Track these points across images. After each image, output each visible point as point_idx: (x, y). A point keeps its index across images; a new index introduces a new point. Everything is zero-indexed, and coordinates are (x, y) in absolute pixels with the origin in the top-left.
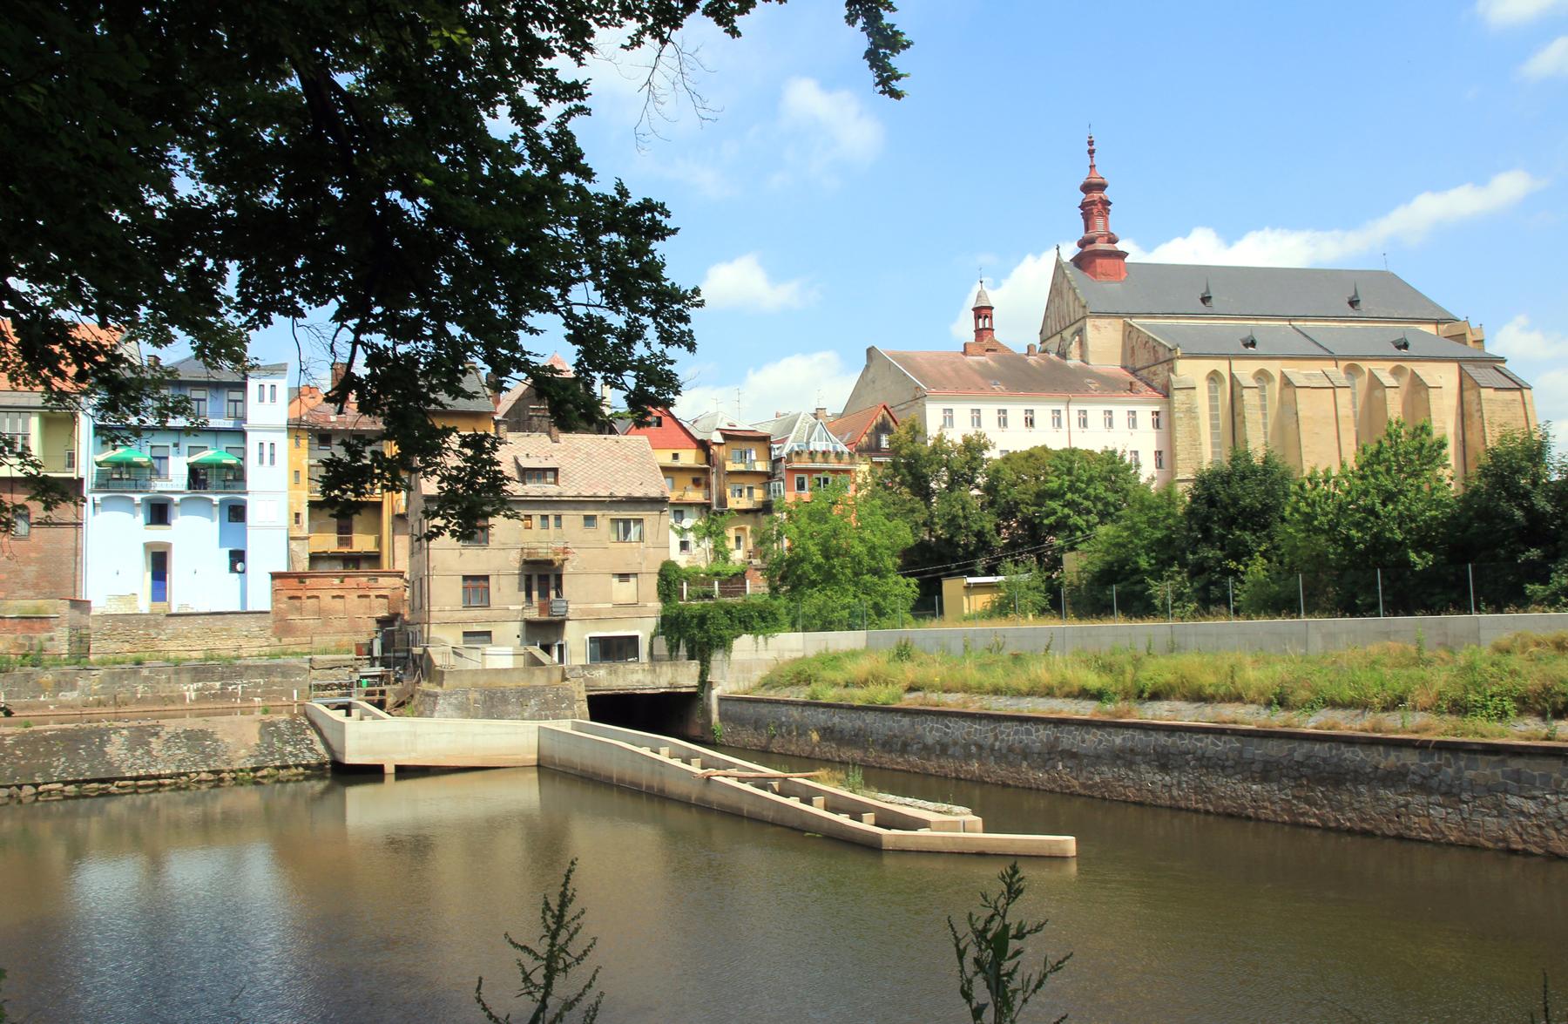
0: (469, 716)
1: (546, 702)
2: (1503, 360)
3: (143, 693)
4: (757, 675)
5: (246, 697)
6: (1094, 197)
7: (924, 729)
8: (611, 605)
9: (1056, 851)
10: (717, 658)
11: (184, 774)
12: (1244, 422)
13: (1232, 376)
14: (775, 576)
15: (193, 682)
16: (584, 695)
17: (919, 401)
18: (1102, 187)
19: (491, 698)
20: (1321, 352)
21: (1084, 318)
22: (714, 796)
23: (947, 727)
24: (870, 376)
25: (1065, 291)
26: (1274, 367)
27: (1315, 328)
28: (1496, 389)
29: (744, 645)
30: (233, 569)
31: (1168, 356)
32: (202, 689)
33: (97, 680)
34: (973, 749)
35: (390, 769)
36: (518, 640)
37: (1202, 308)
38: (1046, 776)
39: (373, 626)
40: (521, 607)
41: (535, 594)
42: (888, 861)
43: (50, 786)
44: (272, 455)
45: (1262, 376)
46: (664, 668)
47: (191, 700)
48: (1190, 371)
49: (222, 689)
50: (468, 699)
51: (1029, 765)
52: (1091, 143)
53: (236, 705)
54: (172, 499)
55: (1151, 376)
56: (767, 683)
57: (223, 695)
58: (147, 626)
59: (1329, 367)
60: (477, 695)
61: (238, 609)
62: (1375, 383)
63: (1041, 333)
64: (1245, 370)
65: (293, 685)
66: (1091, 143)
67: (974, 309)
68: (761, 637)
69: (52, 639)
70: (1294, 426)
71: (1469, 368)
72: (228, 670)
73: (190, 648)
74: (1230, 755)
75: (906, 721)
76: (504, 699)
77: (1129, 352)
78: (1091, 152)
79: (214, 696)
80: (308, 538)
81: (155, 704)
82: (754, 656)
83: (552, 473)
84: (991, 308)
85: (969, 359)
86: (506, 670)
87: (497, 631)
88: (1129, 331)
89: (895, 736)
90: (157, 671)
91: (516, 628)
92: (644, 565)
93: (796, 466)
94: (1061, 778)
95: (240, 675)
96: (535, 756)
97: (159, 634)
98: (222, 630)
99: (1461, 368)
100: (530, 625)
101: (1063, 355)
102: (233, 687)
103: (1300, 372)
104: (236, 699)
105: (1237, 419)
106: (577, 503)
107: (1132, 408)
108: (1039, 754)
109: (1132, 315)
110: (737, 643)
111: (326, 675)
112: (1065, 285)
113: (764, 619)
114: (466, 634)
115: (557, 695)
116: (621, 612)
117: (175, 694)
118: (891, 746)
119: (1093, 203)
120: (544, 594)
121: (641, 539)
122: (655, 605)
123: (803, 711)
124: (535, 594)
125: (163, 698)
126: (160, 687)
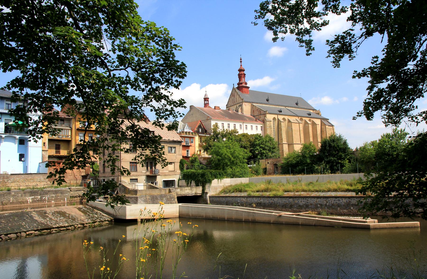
0: (147, 204)
1: (168, 199)
3: (13, 200)
4: (220, 190)
5: (49, 201)
6: (241, 74)
7: (298, 201)
9: (416, 225)
10: (207, 186)
11: (72, 225)
12: (281, 130)
13: (278, 119)
14: (349, 156)
15: (30, 196)
16: (176, 197)
17: (209, 120)
18: (244, 70)
19: (153, 198)
21: (242, 102)
22: (281, 220)
23: (307, 200)
24: (191, 113)
25: (235, 95)
26: (286, 117)
27: (291, 109)
28: (329, 126)
29: (215, 182)
30: (20, 160)
31: (264, 113)
32: (34, 198)
34: (319, 205)
35: (139, 220)
36: (145, 181)
37: (266, 102)
38: (347, 211)
39: (81, 178)
40: (145, 172)
41: (149, 168)
42: (372, 232)
43: (30, 232)
45: (284, 119)
46: (194, 188)
47: (30, 202)
48: (269, 117)
49: (41, 198)
50: (147, 198)
51: (340, 208)
52: (241, 59)
53: (46, 203)
56: (221, 192)
57: (41, 200)
58: (4, 178)
59: (297, 118)
60: (149, 197)
61: (22, 172)
62: (306, 123)
63: (227, 105)
64: (281, 117)
65: (65, 196)
66: (241, 59)
68: (219, 180)
69: (64, 177)
70: (291, 132)
71: (323, 121)
72: (43, 192)
74: (411, 202)
75: (291, 200)
76: (157, 198)
77: (252, 112)
78: (241, 62)
79: (38, 201)
80: (47, 151)
81: (17, 204)
82: (218, 185)
83: (152, 133)
84: (208, 98)
85: (216, 110)
86: (142, 190)
87: (139, 178)
88: (253, 106)
89: (287, 204)
90: (18, 193)
91: (144, 178)
92: (176, 160)
93: (182, 135)
94: (353, 211)
95: (47, 194)
96: (178, 214)
97: (8, 181)
99: (321, 121)
100: (148, 177)
101: (237, 111)
103: (292, 119)
104: (46, 201)
105: (279, 129)
107: (257, 125)
108: (344, 205)
109: (253, 103)
110: (213, 181)
111: (75, 193)
112: (236, 94)
113: (220, 175)
114: (131, 179)
115: (170, 197)
116: (171, 173)
117: (24, 200)
118: (286, 206)
119: (242, 74)
120: (151, 168)
121: (175, 152)
122: (179, 171)
123: (247, 199)
124: (149, 168)
126: (19, 198)
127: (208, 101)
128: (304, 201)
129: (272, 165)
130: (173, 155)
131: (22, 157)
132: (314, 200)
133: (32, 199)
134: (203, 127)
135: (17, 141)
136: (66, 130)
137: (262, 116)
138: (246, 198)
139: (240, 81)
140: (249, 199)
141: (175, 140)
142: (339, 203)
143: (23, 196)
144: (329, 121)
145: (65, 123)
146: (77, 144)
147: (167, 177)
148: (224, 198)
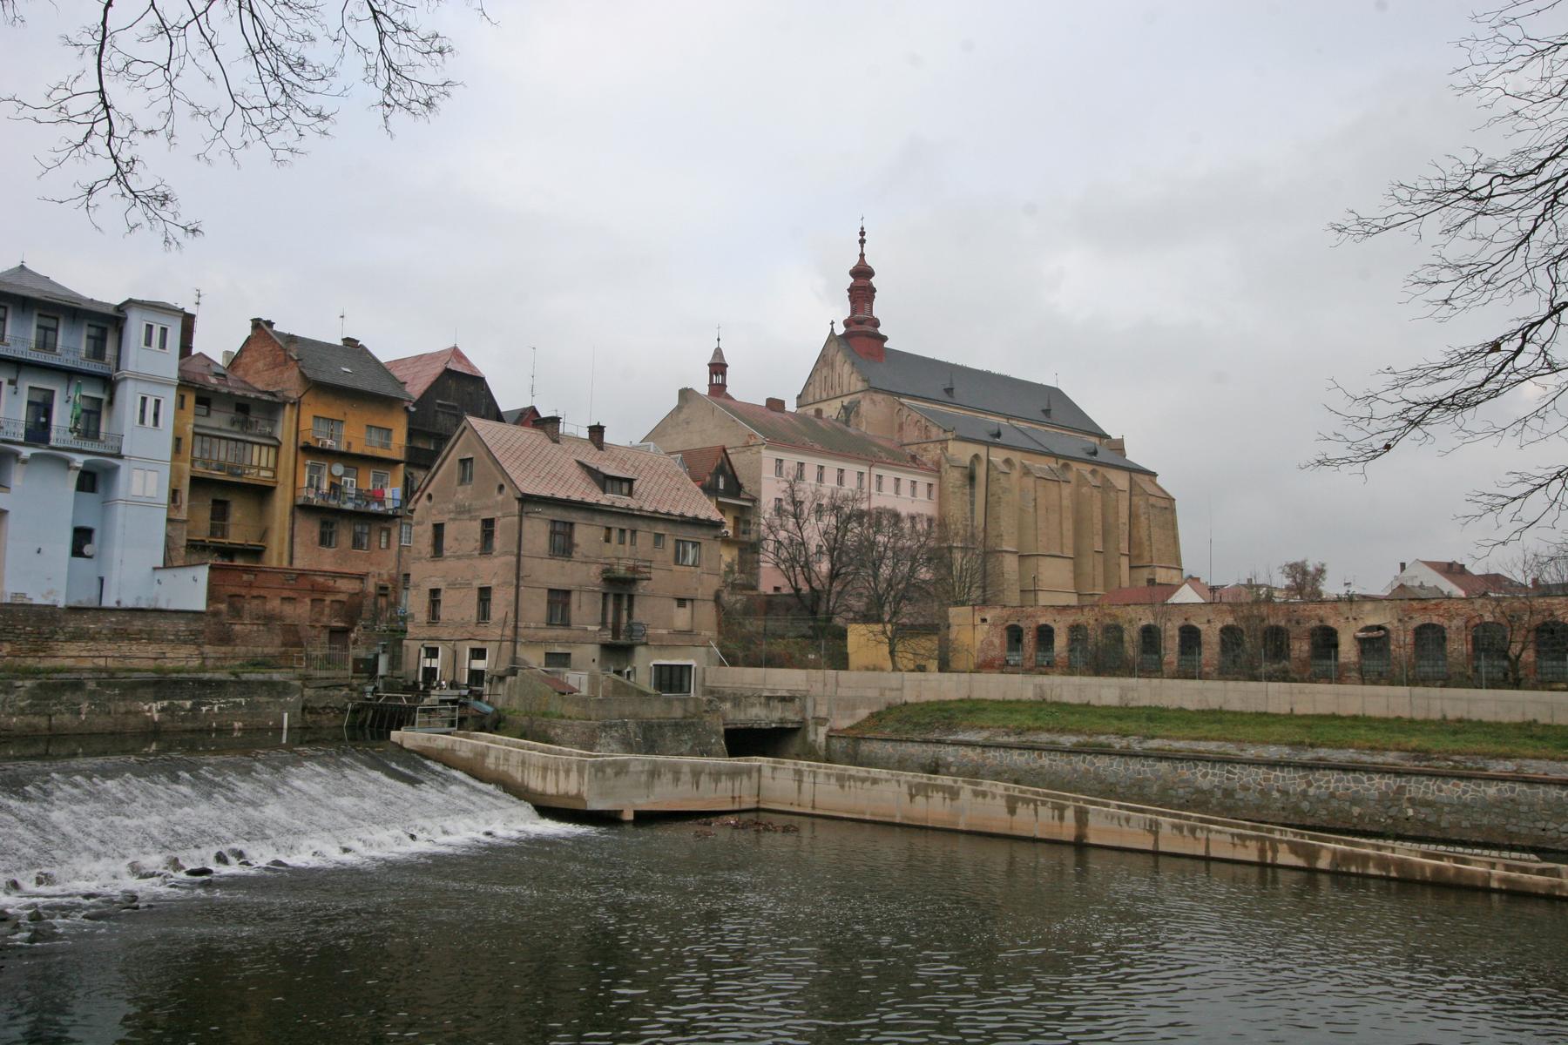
2: (1154, 475)
6: (862, 285)
7: (1194, 774)
13: (988, 460)
16: (722, 729)
20: (1033, 446)
24: (682, 416)
26: (1017, 457)
35: (629, 816)
40: (597, 628)
44: (156, 415)
52: (862, 233)
54: (21, 453)
55: (921, 452)
63: (799, 397)
66: (862, 233)
73: (97, 654)
78: (862, 242)
89: (1148, 779)
91: (593, 651)
98: (141, 631)
99: (1131, 478)
100: (607, 649)
106: (653, 518)
109: (900, 395)
123: (984, 752)
127: (724, 374)
128: (1214, 775)
129: (999, 629)
131: (82, 537)
132: (1257, 774)
133: (163, 710)
134: (730, 473)
135: (73, 478)
136: (200, 438)
138: (979, 750)
139: (853, 311)
140: (991, 753)
141: (701, 517)
142: (1357, 792)
144: (236, 350)
145: (212, 413)
146: (300, 501)
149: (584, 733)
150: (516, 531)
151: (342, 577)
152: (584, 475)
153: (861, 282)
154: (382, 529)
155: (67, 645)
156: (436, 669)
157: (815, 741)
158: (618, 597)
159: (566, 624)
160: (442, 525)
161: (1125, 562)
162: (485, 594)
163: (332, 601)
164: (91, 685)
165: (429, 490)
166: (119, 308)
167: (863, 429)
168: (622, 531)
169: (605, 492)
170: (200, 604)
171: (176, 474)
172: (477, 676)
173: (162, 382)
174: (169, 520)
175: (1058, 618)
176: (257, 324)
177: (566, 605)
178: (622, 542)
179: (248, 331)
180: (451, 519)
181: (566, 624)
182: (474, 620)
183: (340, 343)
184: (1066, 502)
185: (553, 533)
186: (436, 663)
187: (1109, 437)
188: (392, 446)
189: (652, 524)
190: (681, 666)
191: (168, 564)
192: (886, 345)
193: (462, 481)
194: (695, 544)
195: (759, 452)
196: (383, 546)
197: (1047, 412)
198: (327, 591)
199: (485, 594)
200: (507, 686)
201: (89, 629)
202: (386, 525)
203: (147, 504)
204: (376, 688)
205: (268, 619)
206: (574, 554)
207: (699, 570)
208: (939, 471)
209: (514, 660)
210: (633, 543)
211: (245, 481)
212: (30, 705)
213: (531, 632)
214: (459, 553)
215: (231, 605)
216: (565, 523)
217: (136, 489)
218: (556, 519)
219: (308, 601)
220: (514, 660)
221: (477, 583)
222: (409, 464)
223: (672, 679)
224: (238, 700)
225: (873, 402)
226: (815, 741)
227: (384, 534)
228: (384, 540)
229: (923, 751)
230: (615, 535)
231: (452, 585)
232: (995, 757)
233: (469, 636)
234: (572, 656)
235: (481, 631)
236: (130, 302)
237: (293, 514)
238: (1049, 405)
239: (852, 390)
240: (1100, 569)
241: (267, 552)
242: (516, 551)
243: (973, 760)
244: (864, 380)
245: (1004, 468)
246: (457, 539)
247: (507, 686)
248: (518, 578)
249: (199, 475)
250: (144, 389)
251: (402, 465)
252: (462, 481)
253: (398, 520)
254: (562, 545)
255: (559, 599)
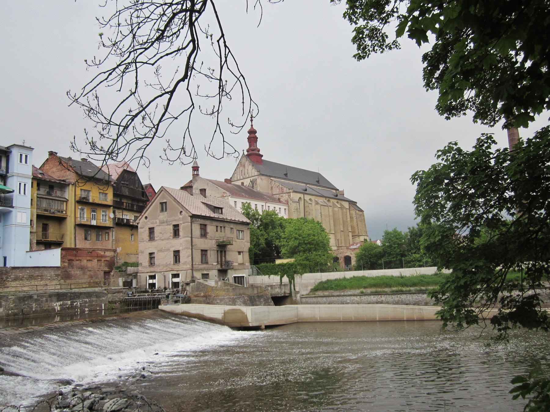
2: (356, 203)
8: (237, 264)
15: (58, 301)
17: (226, 198)
25: (246, 165)
26: (313, 198)
33: (12, 302)
35: (263, 327)
40: (216, 264)
49: (71, 304)
67: (193, 167)
79: (68, 308)
98: (38, 276)
102: (76, 303)
109: (270, 176)
114: (202, 274)
117: (50, 308)
125: (45, 310)
127: (198, 170)
130: (242, 242)
133: (60, 305)
137: (284, 195)
138: (358, 297)
139: (250, 146)
143: (48, 301)
147: (237, 272)
148: (325, 298)
149: (230, 301)
150: (190, 228)
151: (107, 251)
152: (205, 207)
153: (252, 135)
154: (106, 233)
155: (12, 283)
156: (155, 283)
157: (296, 300)
158: (221, 252)
159: (207, 263)
160: (153, 228)
161: (350, 234)
162: (177, 253)
163: (104, 261)
164: (35, 297)
165: (146, 215)
166: (8, 148)
167: (258, 189)
168: (221, 227)
169: (215, 213)
170: (58, 264)
171: (32, 215)
172: (176, 285)
173: (26, 177)
174: (31, 232)
175: (352, 253)
176: (51, 154)
177: (206, 255)
178: (221, 231)
179: (47, 156)
180: (157, 226)
181: (207, 263)
182: (172, 263)
183: (80, 160)
184: (331, 214)
185: (201, 228)
186: (154, 281)
187: (338, 190)
188: (108, 200)
189: (229, 224)
190: (241, 277)
191: (31, 250)
192: (263, 158)
193: (162, 210)
194: (242, 231)
195: (228, 199)
196: (107, 239)
197: (318, 182)
198: (102, 256)
199: (177, 253)
200: (191, 287)
201: (20, 276)
202: (108, 231)
203: (23, 226)
204: (133, 292)
205: (82, 268)
206: (207, 236)
207: (244, 241)
208: (288, 204)
209: (193, 277)
210: (225, 232)
211: (56, 215)
212: (15, 306)
213: (197, 266)
214: (163, 238)
215: (69, 264)
216: (204, 225)
217: (19, 221)
218: (202, 223)
219: (96, 260)
220: (193, 277)
221: (173, 249)
222: (115, 207)
223: (239, 280)
224: (86, 300)
225: (262, 179)
226: (296, 300)
227: (107, 235)
228: (107, 237)
229: (338, 299)
230: (219, 228)
231: (160, 251)
232: (365, 299)
233: (170, 270)
234: (210, 275)
235: (176, 267)
236: (14, 145)
237: (75, 228)
238: (318, 179)
239: (253, 175)
240: (343, 238)
241: (64, 243)
242: (190, 236)
243: (357, 301)
244: (258, 171)
245: (310, 202)
246: (161, 233)
247: (191, 287)
248: (192, 246)
249: (40, 214)
250: (21, 180)
251: (112, 207)
252: (162, 210)
253: (112, 229)
254: (204, 234)
255: (204, 252)
